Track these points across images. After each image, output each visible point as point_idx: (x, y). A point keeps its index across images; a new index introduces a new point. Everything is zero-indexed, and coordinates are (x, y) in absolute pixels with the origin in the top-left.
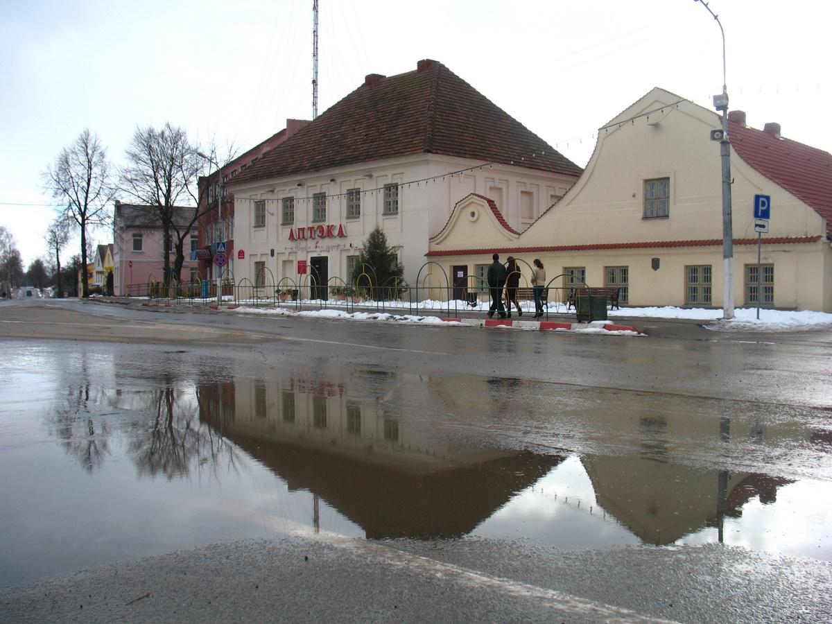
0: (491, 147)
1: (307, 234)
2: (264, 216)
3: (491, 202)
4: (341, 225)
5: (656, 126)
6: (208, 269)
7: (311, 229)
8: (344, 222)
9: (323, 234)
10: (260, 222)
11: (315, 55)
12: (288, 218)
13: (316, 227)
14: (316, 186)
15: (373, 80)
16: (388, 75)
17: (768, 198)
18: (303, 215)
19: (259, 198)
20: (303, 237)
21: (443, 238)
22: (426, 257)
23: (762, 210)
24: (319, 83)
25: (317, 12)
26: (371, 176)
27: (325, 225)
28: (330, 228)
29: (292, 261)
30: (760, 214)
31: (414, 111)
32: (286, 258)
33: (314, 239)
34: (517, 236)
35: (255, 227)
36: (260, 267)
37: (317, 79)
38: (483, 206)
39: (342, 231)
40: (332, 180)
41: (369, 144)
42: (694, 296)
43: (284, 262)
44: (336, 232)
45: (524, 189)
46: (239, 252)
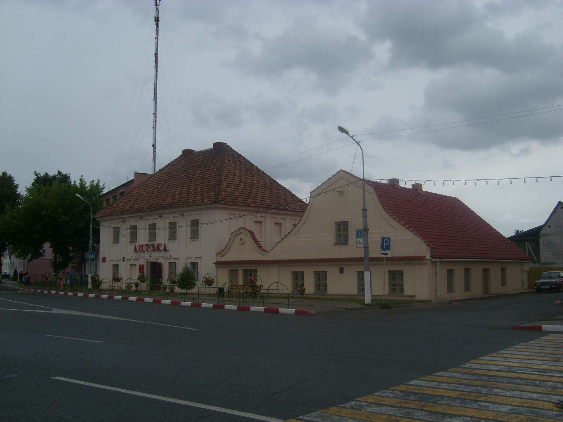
0: (275, 186)
1: (145, 248)
2: (118, 237)
3: (252, 233)
4: (165, 244)
5: (341, 192)
6: (83, 264)
7: (147, 245)
8: (167, 242)
9: (154, 249)
10: (116, 240)
11: (155, 128)
12: (133, 237)
13: (150, 244)
14: (150, 219)
15: (187, 153)
16: (196, 150)
17: (389, 239)
18: (143, 238)
19: (115, 226)
20: (143, 250)
21: (224, 253)
22: (214, 264)
23: (385, 245)
24: (157, 146)
25: (156, 101)
26: (183, 215)
27: (155, 243)
28: (159, 245)
29: (135, 265)
30: (384, 248)
31: (209, 176)
32: (132, 262)
33: (149, 251)
34: (266, 253)
35: (113, 243)
36: (116, 267)
37: (155, 144)
38: (247, 235)
39: (166, 248)
40: (160, 216)
41: (182, 196)
42: (394, 288)
43: (131, 265)
44: (162, 248)
45: (276, 222)
46: (103, 258)
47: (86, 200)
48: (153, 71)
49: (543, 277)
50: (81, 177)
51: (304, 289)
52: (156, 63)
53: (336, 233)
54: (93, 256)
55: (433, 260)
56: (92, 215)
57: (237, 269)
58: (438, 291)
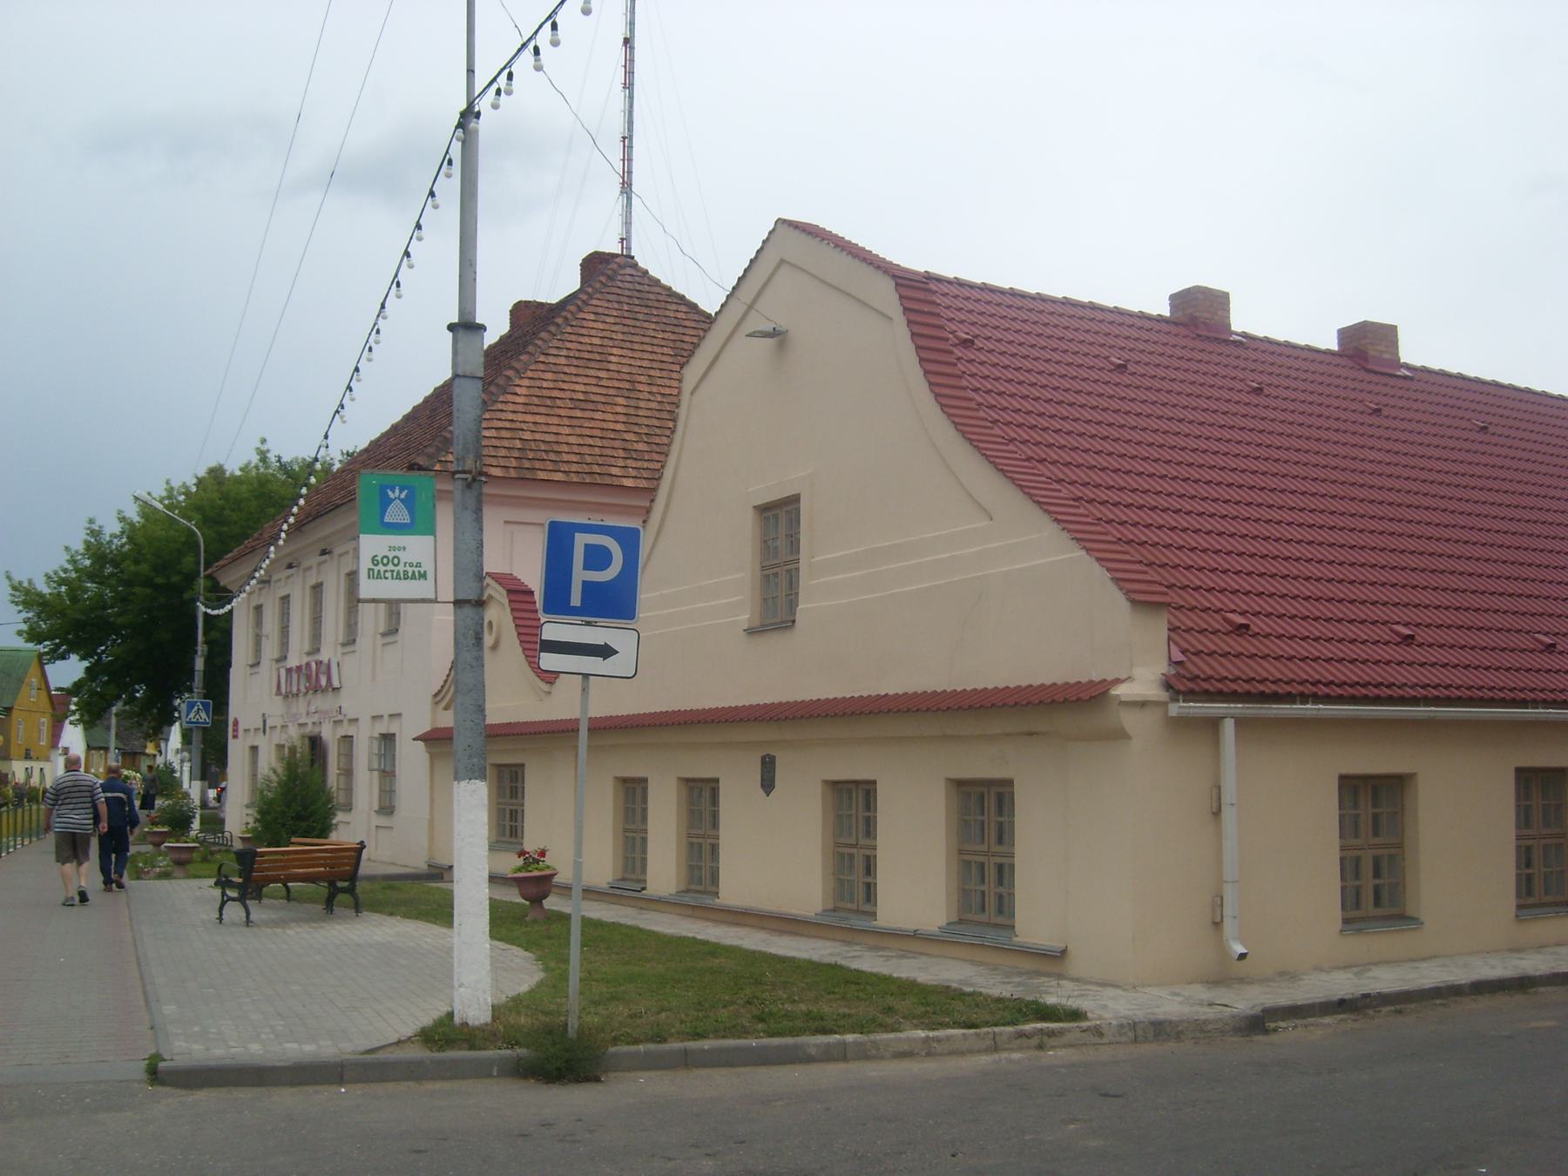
22: (421, 744)
47: (176, 512)
48: (619, 96)
49: (252, 917)
50: (259, 445)
51: (547, 872)
52: (629, 71)
53: (763, 568)
54: (203, 715)
55: (1174, 709)
56: (202, 569)
57: (519, 761)
58: (1229, 927)
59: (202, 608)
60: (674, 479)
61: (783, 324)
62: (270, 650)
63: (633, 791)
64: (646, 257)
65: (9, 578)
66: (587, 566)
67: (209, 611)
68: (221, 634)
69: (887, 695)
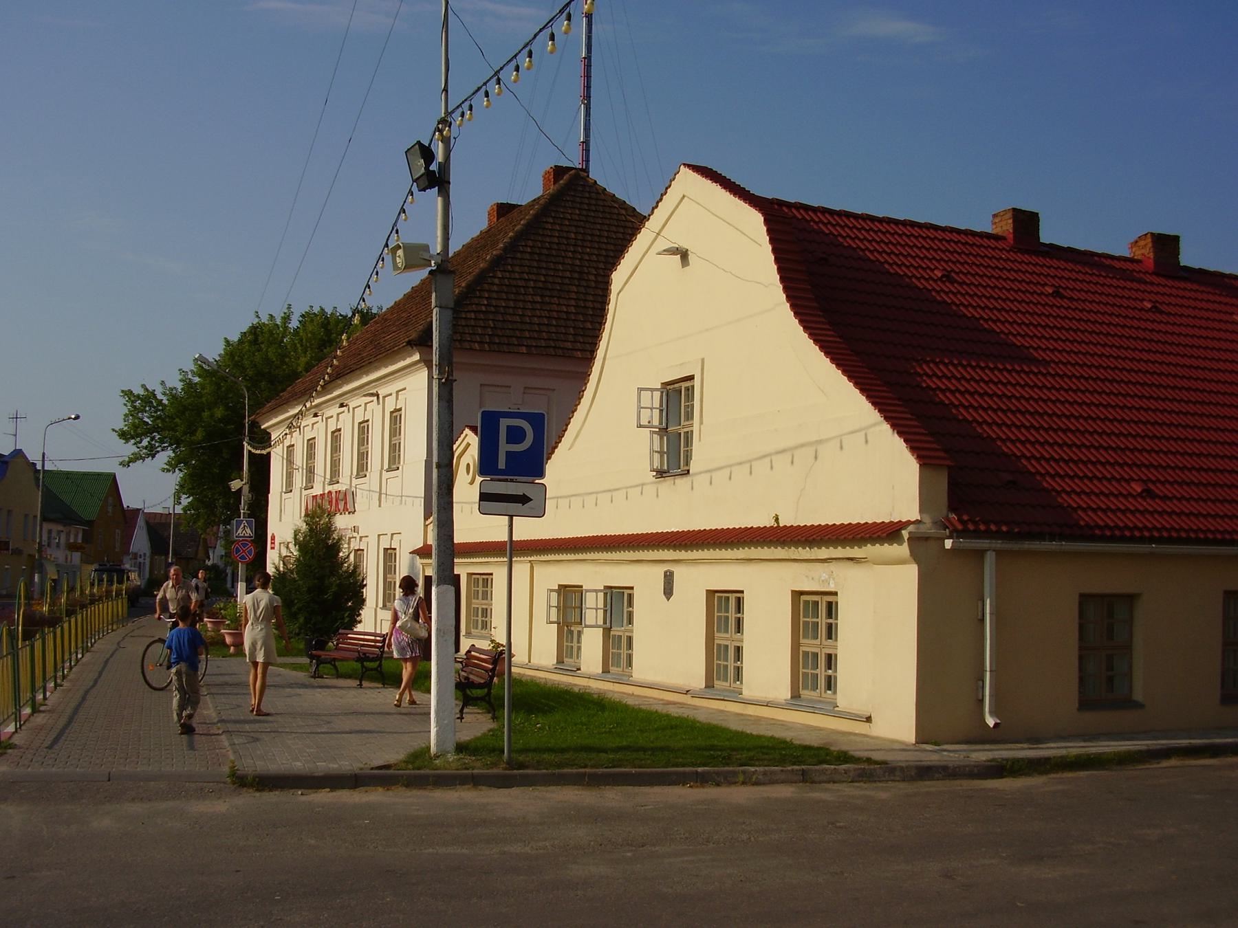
54: (248, 531)
59: (247, 447)
60: (604, 359)
61: (684, 245)
62: (299, 479)
63: (71, 562)
64: (594, 175)
65: (113, 430)
66: (510, 440)
67: (253, 451)
68: (261, 467)
69: (752, 527)
